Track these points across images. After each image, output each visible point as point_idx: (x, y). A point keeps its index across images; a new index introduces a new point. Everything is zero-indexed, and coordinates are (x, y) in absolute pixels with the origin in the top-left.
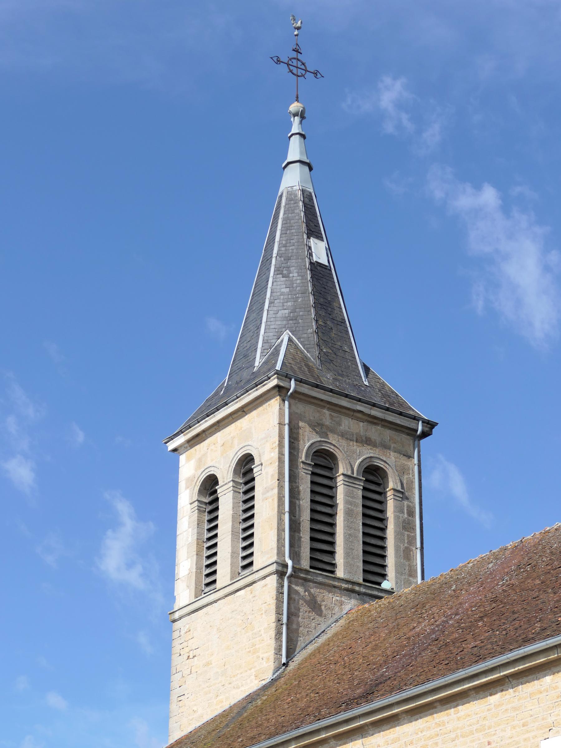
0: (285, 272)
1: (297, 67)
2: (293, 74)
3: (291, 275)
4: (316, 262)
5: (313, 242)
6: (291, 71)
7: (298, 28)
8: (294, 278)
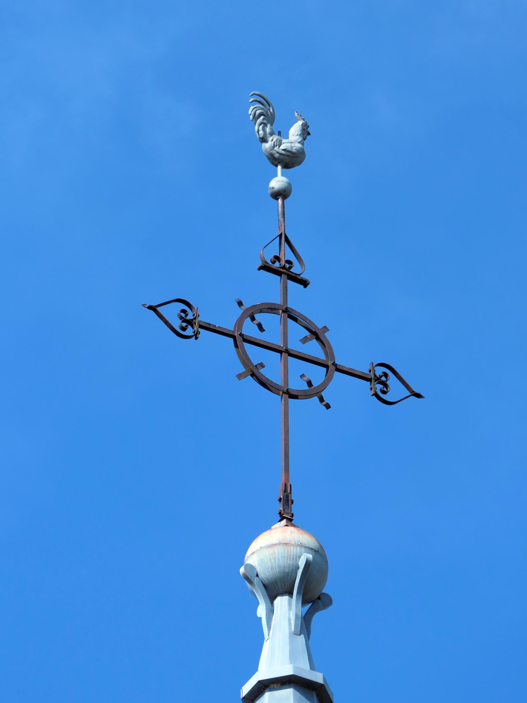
2: (264, 383)
6: (254, 373)
7: (289, 161)
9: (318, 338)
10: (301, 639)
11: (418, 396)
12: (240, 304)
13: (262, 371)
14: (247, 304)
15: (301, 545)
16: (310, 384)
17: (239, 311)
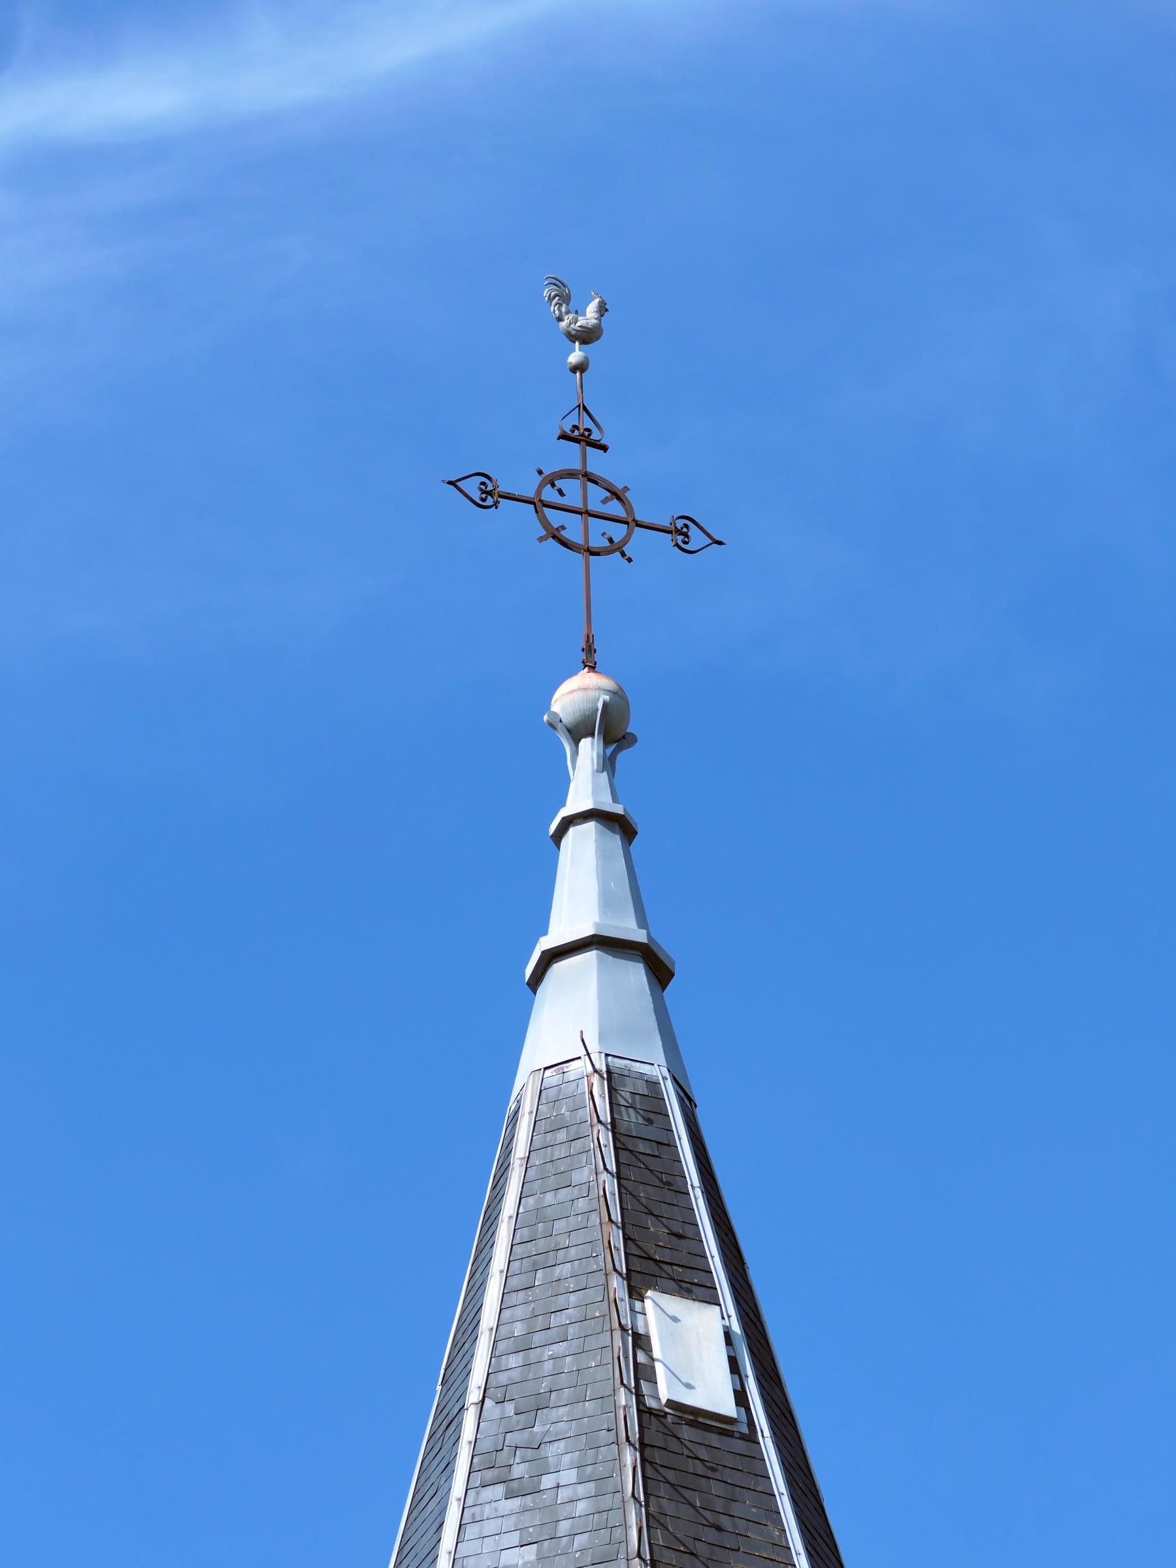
0: (518, 1471)
1: (586, 513)
2: (565, 544)
3: (547, 1481)
4: (670, 1403)
5: (659, 1312)
6: (556, 535)
7: (586, 337)
8: (563, 1495)
9: (619, 498)
10: (604, 776)
11: (720, 543)
12: (540, 472)
13: (563, 533)
14: (546, 472)
15: (600, 689)
16: (611, 540)
17: (540, 478)
